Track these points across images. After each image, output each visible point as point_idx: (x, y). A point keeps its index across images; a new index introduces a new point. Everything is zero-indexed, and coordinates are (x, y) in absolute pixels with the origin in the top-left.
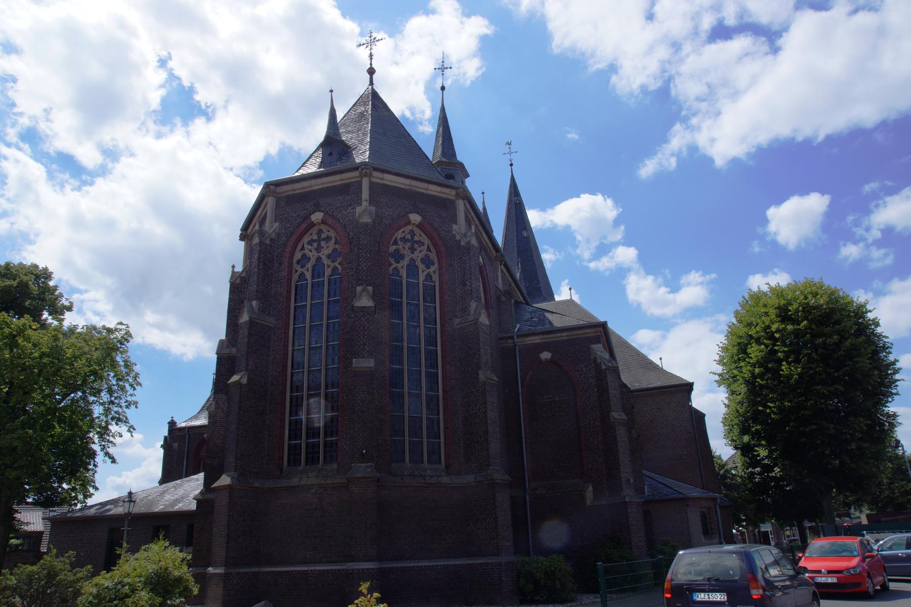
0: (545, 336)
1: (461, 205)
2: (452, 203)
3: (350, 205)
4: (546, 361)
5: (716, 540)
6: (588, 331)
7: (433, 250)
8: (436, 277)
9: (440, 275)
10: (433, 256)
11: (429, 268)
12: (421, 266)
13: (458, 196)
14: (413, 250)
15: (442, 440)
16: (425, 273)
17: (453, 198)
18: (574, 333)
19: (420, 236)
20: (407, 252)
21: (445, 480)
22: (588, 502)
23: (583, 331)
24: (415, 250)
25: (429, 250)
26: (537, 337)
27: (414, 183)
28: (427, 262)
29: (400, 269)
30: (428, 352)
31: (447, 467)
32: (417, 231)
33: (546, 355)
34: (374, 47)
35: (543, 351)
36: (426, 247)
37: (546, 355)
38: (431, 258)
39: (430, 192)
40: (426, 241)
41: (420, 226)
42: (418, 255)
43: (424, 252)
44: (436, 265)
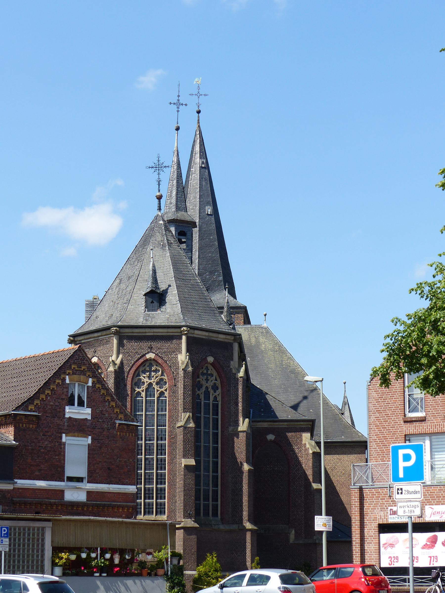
0: (272, 423)
1: (236, 346)
2: (231, 345)
3: (174, 352)
4: (271, 441)
5: (21, 572)
6: (302, 423)
7: (218, 379)
8: (219, 398)
9: (222, 398)
10: (218, 383)
11: (215, 392)
12: (212, 392)
13: (235, 340)
14: (207, 380)
15: (219, 503)
16: (214, 396)
17: (232, 342)
18: (292, 423)
19: (212, 370)
20: (204, 382)
21: (222, 527)
22: (291, 541)
23: (299, 423)
24: (208, 380)
25: (216, 380)
26: (266, 424)
27: (211, 334)
28: (215, 388)
29: (200, 394)
30: (214, 448)
31: (222, 519)
32: (210, 367)
33: (271, 437)
34: (161, 172)
35: (269, 434)
36: (214, 378)
37: (271, 437)
38: (217, 385)
39: (219, 340)
40: (215, 374)
41: (212, 364)
42: (210, 384)
43: (214, 381)
44: (220, 390)
